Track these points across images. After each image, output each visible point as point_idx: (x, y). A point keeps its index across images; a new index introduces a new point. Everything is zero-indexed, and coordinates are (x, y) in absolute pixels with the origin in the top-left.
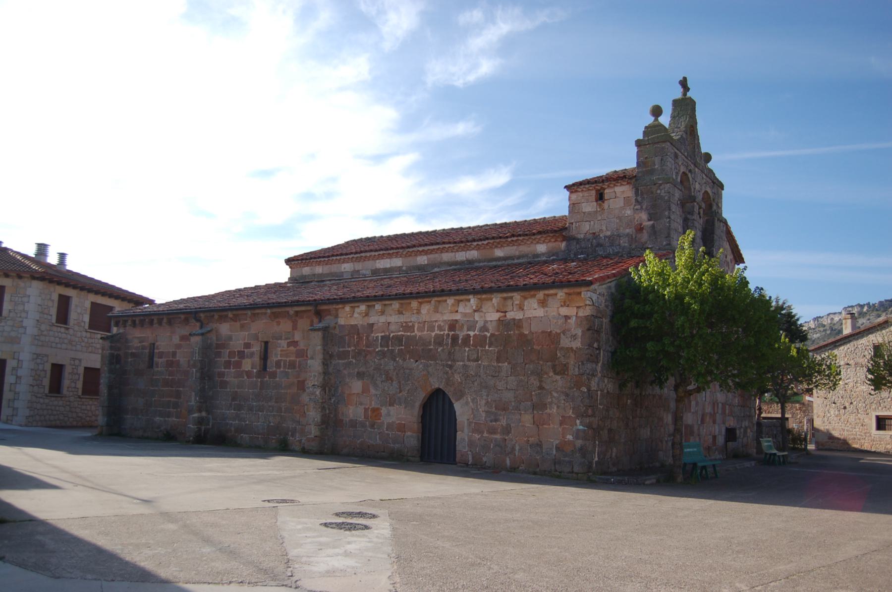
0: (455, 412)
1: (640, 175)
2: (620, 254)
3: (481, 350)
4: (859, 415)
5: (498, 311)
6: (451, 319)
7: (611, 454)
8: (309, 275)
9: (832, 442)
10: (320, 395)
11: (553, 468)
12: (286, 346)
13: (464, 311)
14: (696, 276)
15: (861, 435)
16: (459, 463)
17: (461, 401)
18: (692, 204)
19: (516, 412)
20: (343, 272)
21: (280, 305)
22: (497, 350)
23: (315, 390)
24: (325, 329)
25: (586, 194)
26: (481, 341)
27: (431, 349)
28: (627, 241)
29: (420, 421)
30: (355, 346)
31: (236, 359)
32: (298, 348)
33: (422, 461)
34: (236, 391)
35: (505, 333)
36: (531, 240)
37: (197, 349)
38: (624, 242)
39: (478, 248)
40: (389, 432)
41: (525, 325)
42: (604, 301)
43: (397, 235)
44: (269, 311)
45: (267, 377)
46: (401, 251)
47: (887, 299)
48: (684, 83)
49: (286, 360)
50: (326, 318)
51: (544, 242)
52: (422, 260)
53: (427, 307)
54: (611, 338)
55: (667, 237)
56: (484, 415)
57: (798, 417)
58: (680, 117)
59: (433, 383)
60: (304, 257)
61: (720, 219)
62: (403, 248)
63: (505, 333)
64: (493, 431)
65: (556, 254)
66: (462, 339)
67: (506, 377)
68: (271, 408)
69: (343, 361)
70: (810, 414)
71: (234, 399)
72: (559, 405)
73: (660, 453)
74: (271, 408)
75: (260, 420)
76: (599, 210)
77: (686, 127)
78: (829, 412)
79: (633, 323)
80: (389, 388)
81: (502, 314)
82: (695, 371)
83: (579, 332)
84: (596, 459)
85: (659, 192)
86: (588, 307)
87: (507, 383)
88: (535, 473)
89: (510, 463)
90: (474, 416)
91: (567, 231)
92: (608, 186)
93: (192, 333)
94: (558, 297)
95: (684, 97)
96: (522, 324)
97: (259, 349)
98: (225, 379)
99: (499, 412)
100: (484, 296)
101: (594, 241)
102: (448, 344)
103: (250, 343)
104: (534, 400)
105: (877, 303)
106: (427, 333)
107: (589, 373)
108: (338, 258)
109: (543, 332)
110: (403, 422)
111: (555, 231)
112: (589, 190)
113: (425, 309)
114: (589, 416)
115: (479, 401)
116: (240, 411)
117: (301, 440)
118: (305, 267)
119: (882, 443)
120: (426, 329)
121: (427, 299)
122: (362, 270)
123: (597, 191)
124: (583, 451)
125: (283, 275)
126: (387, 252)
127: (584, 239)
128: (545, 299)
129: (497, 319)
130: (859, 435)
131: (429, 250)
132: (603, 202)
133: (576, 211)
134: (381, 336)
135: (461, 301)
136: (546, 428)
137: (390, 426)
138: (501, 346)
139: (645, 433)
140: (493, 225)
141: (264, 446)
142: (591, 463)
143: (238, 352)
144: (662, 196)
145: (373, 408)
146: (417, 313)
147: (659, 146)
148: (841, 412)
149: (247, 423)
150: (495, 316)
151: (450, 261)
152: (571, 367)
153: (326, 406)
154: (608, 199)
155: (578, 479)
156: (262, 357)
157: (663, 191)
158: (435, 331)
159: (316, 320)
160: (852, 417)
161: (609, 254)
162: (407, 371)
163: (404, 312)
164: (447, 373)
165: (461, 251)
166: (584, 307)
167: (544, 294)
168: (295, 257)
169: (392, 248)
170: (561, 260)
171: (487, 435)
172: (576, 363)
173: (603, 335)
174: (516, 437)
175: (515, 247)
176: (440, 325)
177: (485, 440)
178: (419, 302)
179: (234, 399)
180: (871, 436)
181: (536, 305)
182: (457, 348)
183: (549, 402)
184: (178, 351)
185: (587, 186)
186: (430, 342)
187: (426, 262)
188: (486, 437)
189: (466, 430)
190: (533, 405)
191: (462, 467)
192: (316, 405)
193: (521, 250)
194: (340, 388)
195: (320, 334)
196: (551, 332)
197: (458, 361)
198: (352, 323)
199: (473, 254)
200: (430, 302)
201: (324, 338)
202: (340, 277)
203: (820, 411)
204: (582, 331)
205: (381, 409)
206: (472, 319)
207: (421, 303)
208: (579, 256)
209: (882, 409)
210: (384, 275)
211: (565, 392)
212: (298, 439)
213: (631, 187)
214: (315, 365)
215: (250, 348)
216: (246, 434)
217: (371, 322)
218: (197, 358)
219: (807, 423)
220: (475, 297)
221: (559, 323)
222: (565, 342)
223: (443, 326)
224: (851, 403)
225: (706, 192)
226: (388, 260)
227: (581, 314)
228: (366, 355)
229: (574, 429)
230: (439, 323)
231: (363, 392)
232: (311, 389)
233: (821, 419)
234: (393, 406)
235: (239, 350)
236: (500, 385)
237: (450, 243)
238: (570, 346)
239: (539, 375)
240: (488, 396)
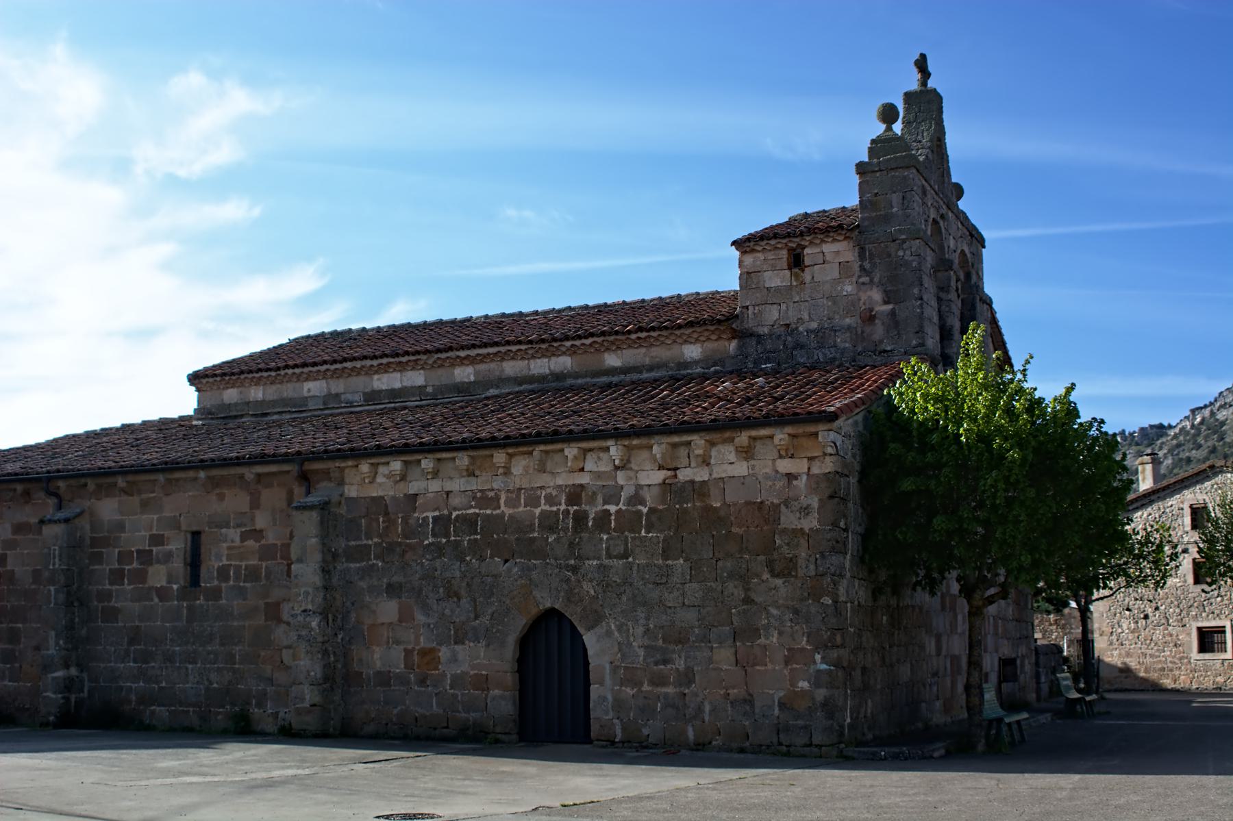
0: (585, 650)
1: (866, 223)
2: (837, 363)
3: (631, 538)
4: (1170, 628)
5: (660, 468)
6: (571, 482)
7: (866, 710)
8: (236, 404)
9: (1126, 677)
10: (320, 627)
11: (775, 740)
12: (238, 539)
13: (596, 469)
14: (1004, 401)
15: (1175, 663)
16: (598, 740)
17: (596, 630)
18: (946, 273)
19: (703, 644)
20: (306, 398)
21: (225, 463)
22: (662, 536)
23: (308, 619)
24: (324, 507)
25: (770, 256)
26: (630, 521)
27: (535, 538)
28: (848, 340)
29: (516, 669)
30: (380, 536)
31: (135, 565)
32: (263, 542)
33: (521, 740)
34: (138, 626)
35: (677, 506)
36: (673, 337)
37: (57, 548)
38: (843, 341)
39: (572, 352)
40: (456, 692)
41: (714, 491)
42: (850, 448)
43: (394, 326)
44: (202, 474)
45: (202, 598)
46: (424, 357)
47: (1152, 423)
48: (922, 65)
49: (241, 566)
50: (318, 486)
51: (697, 340)
52: (464, 374)
53: (524, 463)
54: (860, 511)
55: (917, 332)
56: (641, 652)
57: (1053, 637)
58: (920, 123)
59: (541, 600)
60: (227, 370)
61: (984, 298)
62: (427, 352)
63: (677, 506)
64: (658, 681)
65: (721, 362)
66: (593, 519)
67: (681, 584)
68: (212, 656)
69: (358, 565)
70: (1072, 631)
71: (132, 641)
72: (783, 629)
73: (923, 705)
74: (212, 656)
75: (191, 677)
76: (795, 283)
77: (931, 141)
78: (1120, 626)
79: (907, 485)
80: (452, 611)
81: (669, 473)
82: (1015, 563)
83: (815, 502)
84: (848, 720)
85: (901, 253)
86: (828, 459)
87: (683, 595)
88: (742, 751)
89: (695, 735)
90: (623, 655)
91: (739, 322)
92: (811, 243)
93: (46, 519)
94: (776, 440)
95: (923, 88)
96: (709, 490)
97: (183, 546)
98: (112, 604)
99: (672, 647)
100: (635, 442)
101: (789, 339)
102: (568, 528)
103: (163, 535)
104: (735, 623)
105: (1137, 430)
106: (525, 509)
107: (835, 572)
108: (297, 371)
109: (748, 503)
110: (484, 672)
111: (719, 322)
112: (777, 248)
113: (519, 466)
114: (838, 647)
115: (631, 628)
116: (147, 663)
117: (277, 713)
118: (227, 388)
119: (1209, 673)
120: (522, 501)
121: (525, 449)
122: (344, 393)
123: (790, 250)
124: (829, 708)
125: (184, 402)
126: (397, 360)
127: (771, 335)
128: (749, 446)
129: (660, 481)
130: (1171, 662)
131: (478, 355)
132: (803, 271)
133: (754, 286)
134: (433, 517)
135: (590, 450)
136: (759, 670)
137: (457, 681)
138: (669, 530)
139: (904, 672)
140: (582, 308)
141: (200, 726)
142: (842, 727)
143: (138, 552)
144: (907, 261)
145: (423, 648)
146: (505, 474)
147: (897, 174)
148: (1139, 625)
149: (164, 684)
150: (658, 477)
151: (519, 375)
152: (801, 563)
153: (331, 649)
154: (809, 266)
155: (821, 757)
156: (189, 560)
157: (908, 252)
158: (540, 506)
159: (298, 490)
160: (1158, 632)
161: (818, 362)
162: (489, 579)
163: (477, 473)
164: (568, 580)
165: (539, 358)
166: (822, 458)
167: (750, 437)
168: (206, 369)
169: (407, 353)
170: (731, 373)
171: (649, 688)
172: (810, 556)
173: (850, 505)
174: (705, 690)
175: (643, 350)
176: (551, 494)
177: (645, 697)
178: (507, 454)
179: (132, 641)
180: (1190, 662)
181: (732, 457)
182: (585, 535)
183: (762, 625)
184: (8, 552)
185: (773, 242)
186: (532, 525)
187: (472, 378)
188: (647, 691)
189: (608, 681)
190: (735, 633)
191: (603, 747)
192: (311, 646)
193: (654, 354)
194: (353, 616)
195: (315, 515)
196: (762, 502)
197: (588, 559)
198: (375, 495)
199: (564, 363)
200: (530, 453)
201: (322, 522)
202: (300, 407)
203: (1105, 624)
204: (820, 500)
205: (439, 650)
206: (611, 483)
207: (511, 456)
208: (763, 366)
209: (1208, 616)
210: (390, 403)
211: (793, 606)
212: (271, 711)
213: (851, 244)
214: (308, 573)
215: (163, 545)
216: (163, 706)
217: (411, 492)
218: (57, 566)
219: (1068, 647)
220: (619, 443)
221: (777, 488)
222: (789, 520)
223: (556, 496)
224: (1157, 609)
225: (963, 251)
226: (398, 375)
227: (816, 470)
228: (404, 552)
229: (811, 671)
230: (549, 491)
231: (400, 621)
232: (300, 618)
233: (1106, 638)
234: (463, 643)
235: (141, 548)
236: (671, 599)
237: (520, 343)
238: (799, 527)
239: (744, 578)
240: (647, 619)
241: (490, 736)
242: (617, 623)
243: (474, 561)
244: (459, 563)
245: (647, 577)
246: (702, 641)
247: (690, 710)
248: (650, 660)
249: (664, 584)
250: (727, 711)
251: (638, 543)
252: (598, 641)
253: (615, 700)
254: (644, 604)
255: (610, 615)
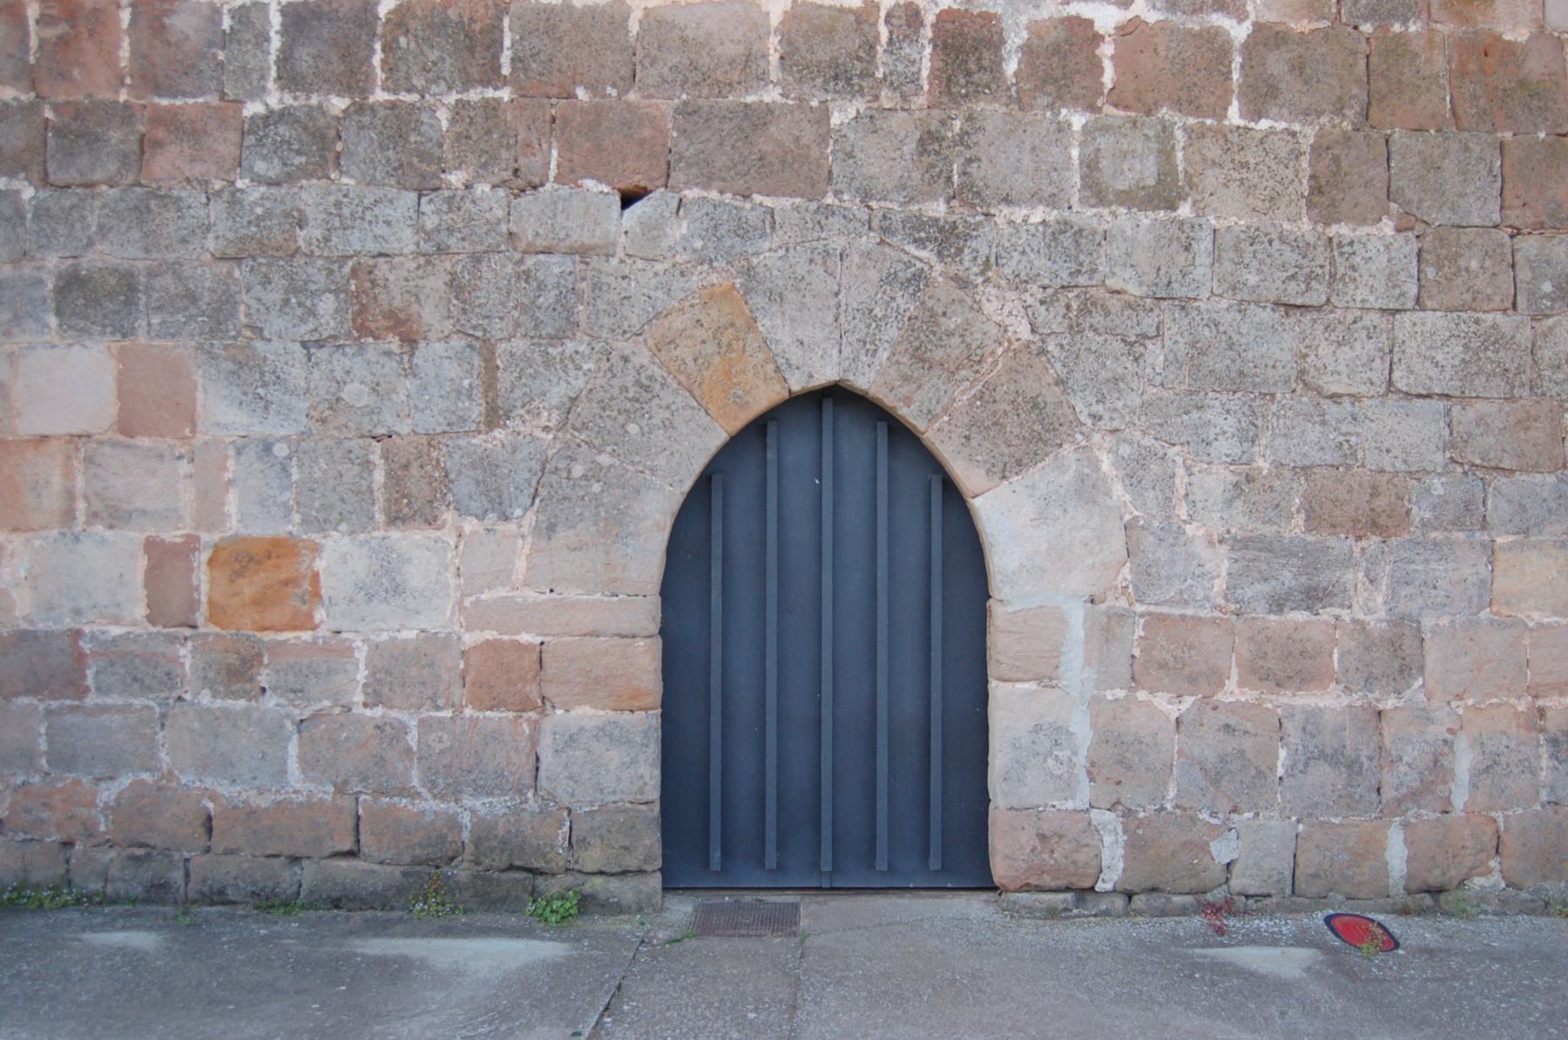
16: (1027, 888)
17: (1034, 474)
19: (1461, 536)
22: (1308, 135)
27: (769, 109)
35: (1367, 28)
56: (1220, 563)
59: (795, 354)
63: (1367, 28)
89: (1409, 860)
99: (1340, 544)
102: (915, 80)
110: (525, 638)
115: (1180, 471)
138: (1339, 111)
145: (236, 539)
164: (918, 280)
171: (1249, 695)
182: (990, 110)
188: (1233, 707)
189: (1076, 667)
191: (1052, 913)
197: (1007, 200)
204: (796, 924)
205: (316, 549)
228: (145, 147)
231: (126, 427)
234: (431, 521)
241: (551, 886)
242: (1125, 450)
243: (482, 188)
244: (413, 196)
245: (1253, 279)
246: (1457, 524)
247: (1403, 768)
248: (1254, 590)
249: (1319, 308)
250: (1533, 773)
251: (1213, 150)
252: (1042, 517)
253: (1106, 738)
254: (1237, 382)
255: (1096, 418)
